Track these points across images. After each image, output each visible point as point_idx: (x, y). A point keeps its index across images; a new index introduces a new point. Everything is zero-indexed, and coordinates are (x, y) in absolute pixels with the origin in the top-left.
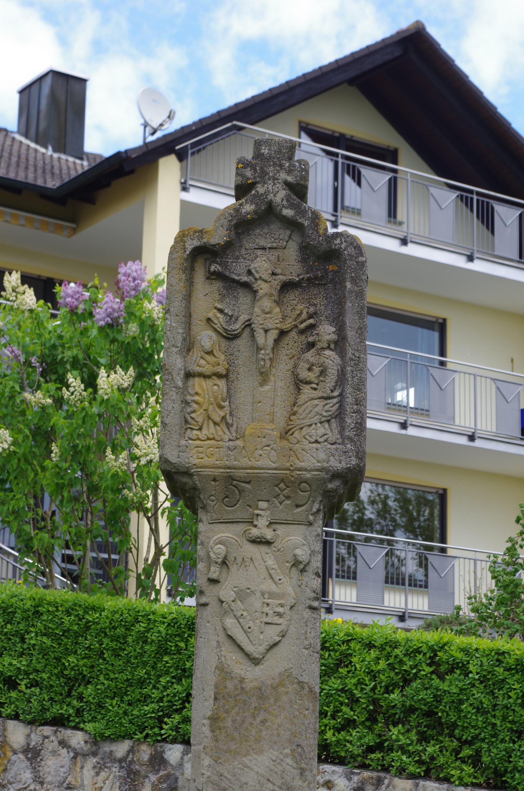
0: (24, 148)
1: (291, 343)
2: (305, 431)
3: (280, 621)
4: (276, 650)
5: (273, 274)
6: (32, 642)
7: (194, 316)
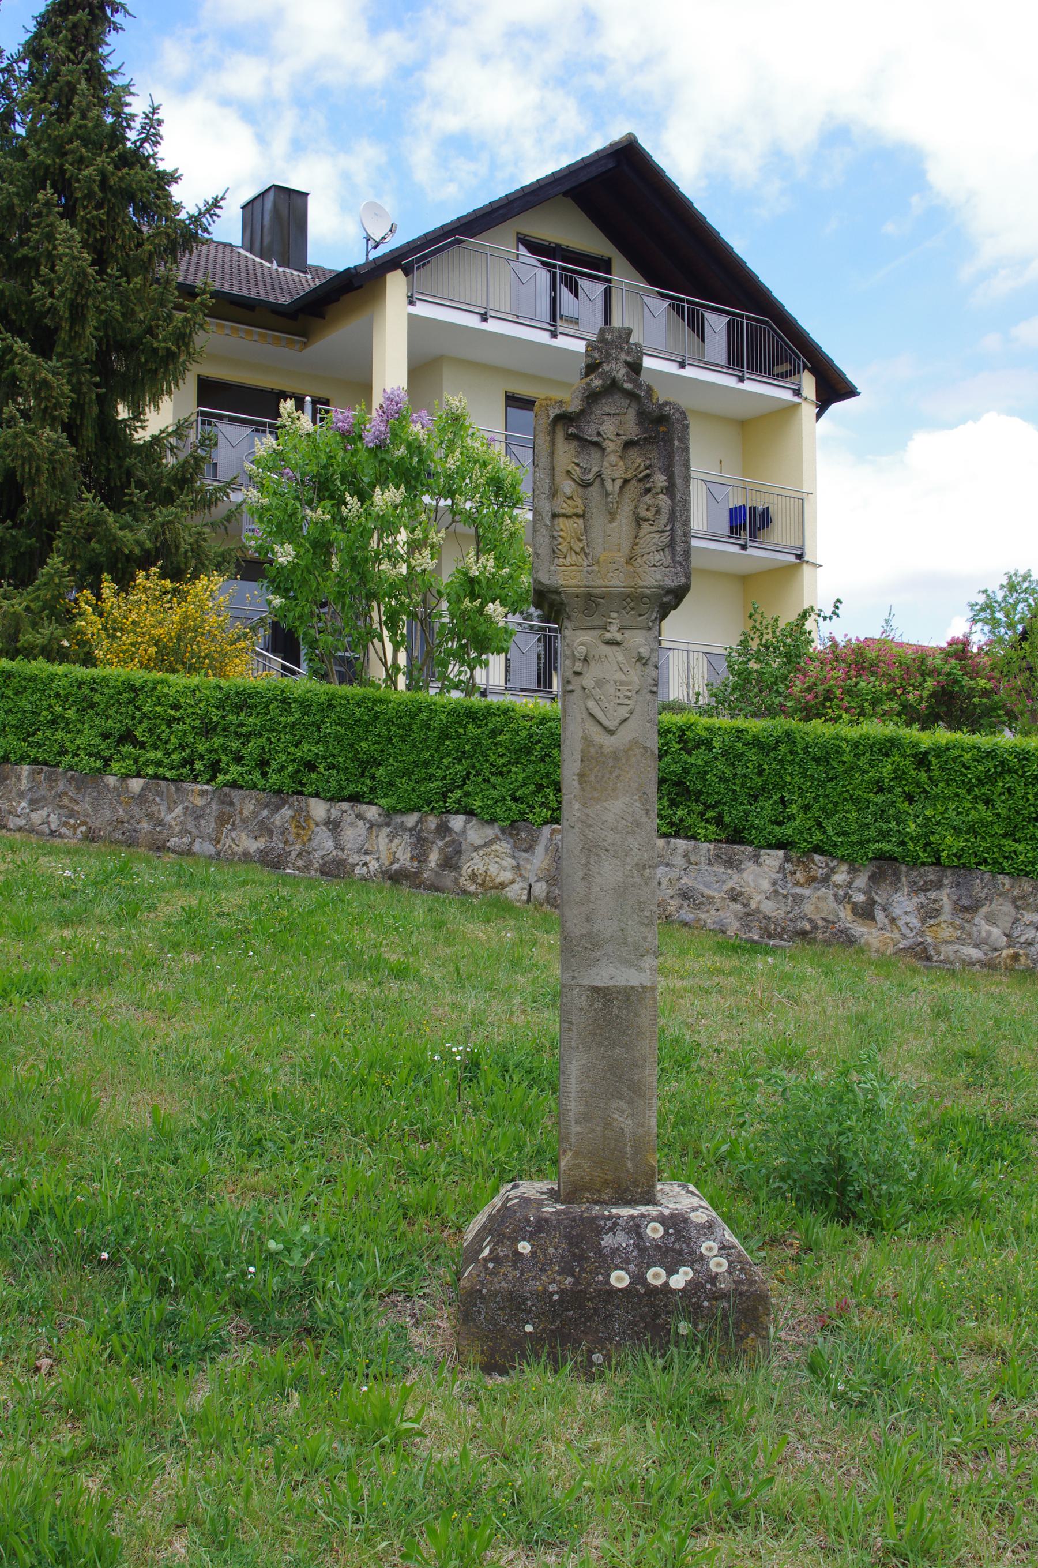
0: (250, 263)
1: (632, 489)
2: (645, 557)
3: (629, 702)
4: (626, 724)
5: (618, 435)
6: (328, 731)
7: (557, 469)
